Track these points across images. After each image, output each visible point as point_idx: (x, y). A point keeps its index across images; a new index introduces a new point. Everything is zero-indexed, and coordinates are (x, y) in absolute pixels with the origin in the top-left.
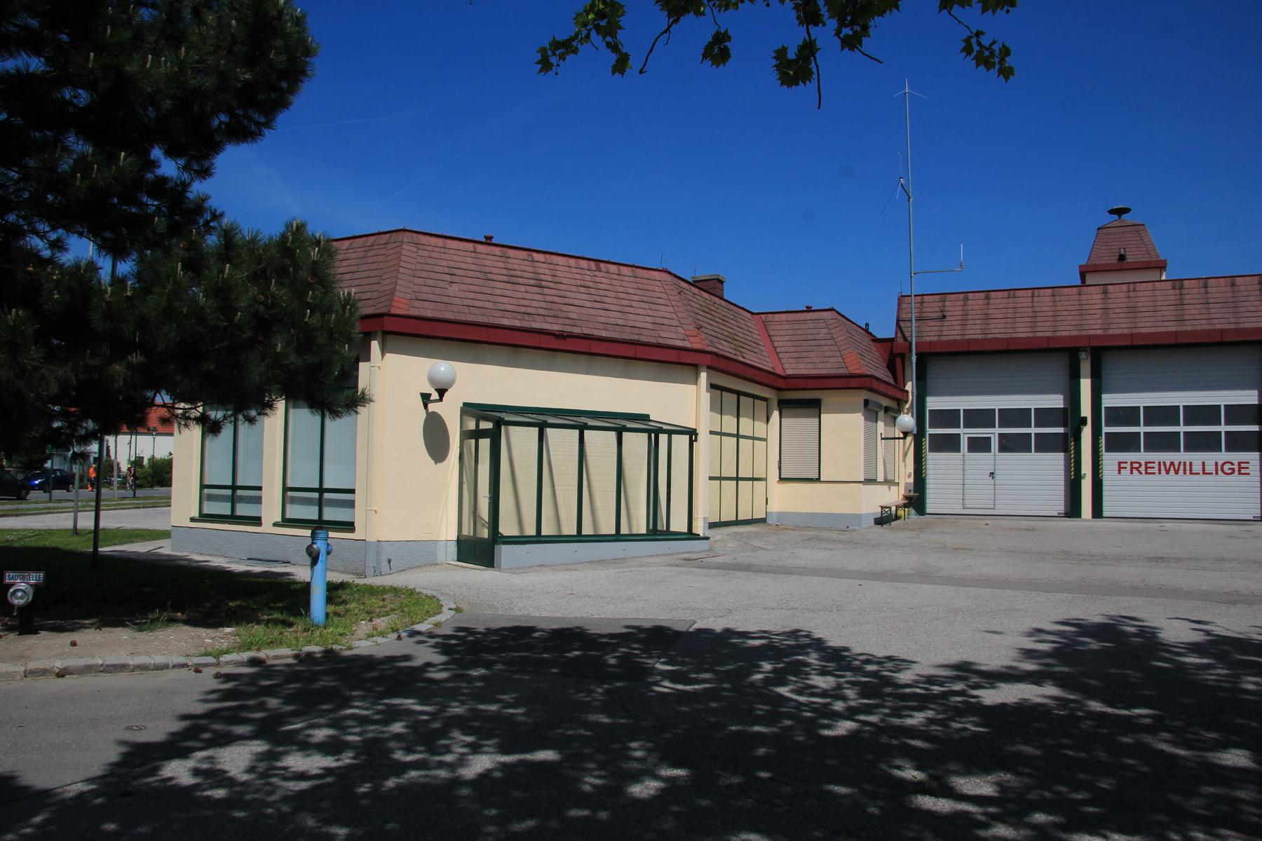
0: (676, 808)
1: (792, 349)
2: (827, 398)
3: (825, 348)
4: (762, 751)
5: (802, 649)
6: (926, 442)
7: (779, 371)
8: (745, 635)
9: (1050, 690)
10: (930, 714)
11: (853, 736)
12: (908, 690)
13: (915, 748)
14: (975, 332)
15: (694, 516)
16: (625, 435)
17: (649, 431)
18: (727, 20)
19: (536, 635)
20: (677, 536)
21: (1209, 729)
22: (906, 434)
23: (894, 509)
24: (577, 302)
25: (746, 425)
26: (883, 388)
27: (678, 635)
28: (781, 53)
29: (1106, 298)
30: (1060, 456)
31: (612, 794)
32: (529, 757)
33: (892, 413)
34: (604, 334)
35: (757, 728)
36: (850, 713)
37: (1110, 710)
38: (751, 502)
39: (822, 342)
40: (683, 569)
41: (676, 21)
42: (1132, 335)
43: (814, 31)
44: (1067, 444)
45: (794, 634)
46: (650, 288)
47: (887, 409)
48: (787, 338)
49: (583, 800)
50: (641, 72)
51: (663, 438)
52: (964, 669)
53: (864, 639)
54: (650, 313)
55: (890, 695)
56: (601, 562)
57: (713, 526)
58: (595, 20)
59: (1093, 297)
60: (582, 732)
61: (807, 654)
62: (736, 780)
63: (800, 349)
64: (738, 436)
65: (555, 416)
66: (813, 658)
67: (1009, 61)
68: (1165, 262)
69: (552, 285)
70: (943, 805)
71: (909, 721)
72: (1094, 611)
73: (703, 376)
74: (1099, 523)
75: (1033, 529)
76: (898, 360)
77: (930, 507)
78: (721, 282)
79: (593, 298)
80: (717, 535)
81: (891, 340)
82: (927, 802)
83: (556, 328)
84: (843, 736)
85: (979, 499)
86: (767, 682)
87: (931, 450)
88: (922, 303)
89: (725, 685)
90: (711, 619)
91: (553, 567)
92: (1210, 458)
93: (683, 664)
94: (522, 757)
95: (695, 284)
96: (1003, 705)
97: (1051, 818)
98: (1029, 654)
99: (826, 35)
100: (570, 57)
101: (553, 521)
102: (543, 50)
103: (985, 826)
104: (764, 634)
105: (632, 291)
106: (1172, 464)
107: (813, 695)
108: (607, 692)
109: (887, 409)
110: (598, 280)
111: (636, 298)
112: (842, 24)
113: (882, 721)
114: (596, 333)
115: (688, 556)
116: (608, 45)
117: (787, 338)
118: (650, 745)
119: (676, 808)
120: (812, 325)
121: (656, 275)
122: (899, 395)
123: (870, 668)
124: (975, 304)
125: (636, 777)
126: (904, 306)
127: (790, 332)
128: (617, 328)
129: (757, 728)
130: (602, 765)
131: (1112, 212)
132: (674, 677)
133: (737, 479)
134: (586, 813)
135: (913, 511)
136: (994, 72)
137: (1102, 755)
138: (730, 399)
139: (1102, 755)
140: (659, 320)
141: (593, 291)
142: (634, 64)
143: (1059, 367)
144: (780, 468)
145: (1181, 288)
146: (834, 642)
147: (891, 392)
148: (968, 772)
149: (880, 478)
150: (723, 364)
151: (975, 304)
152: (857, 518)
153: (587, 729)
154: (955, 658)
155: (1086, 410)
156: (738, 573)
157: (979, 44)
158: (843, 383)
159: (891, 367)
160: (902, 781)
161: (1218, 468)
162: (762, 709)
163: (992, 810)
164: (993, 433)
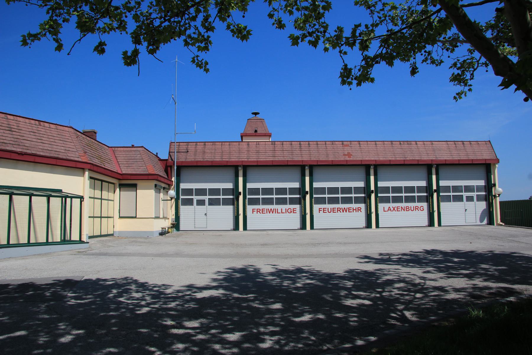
0: (80, 344)
1: (125, 163)
2: (140, 183)
3: (139, 163)
4: (113, 321)
5: (129, 284)
6: (180, 202)
7: (119, 172)
8: (105, 280)
9: (221, 291)
10: (177, 303)
11: (149, 312)
12: (170, 296)
13: (172, 314)
14: (199, 158)
15: (82, 233)
16: (51, 198)
17: (62, 197)
18: (105, 37)
19: (10, 287)
20: (75, 242)
21: (271, 299)
22: (172, 198)
23: (167, 229)
24: (29, 139)
25: (105, 194)
26: (162, 180)
27: (77, 282)
28: (125, 53)
29: (248, 147)
30: (231, 207)
31: (53, 342)
32: (12, 335)
33: (166, 190)
34: (42, 154)
35: (111, 313)
36: (148, 305)
37: (240, 296)
38: (107, 227)
39: (138, 160)
40: (78, 256)
41: (85, 35)
42: (257, 161)
43: (138, 47)
44: (234, 202)
45: (126, 278)
46: (63, 134)
47: (164, 188)
48: (123, 158)
49: (39, 347)
50: (68, 54)
51: (68, 200)
52: (190, 287)
53: (153, 279)
54: (63, 145)
55: (163, 297)
56: (40, 255)
57: (90, 237)
58: (49, 28)
59: (244, 146)
60: (37, 322)
61: (131, 286)
62: (103, 332)
63: (128, 163)
64: (101, 199)
65: (17, 190)
66: (133, 287)
67: (208, 67)
68: (271, 134)
69: (17, 130)
70: (181, 331)
71: (170, 306)
72: (239, 264)
73: (87, 173)
74: (246, 232)
75: (221, 235)
76: (169, 168)
77: (182, 227)
78: (96, 133)
79: (37, 137)
80: (92, 241)
81: (167, 160)
82: (175, 331)
83: (18, 150)
84: (145, 313)
85: (201, 224)
86: (115, 297)
87: (182, 205)
88: (179, 145)
89: (98, 299)
90: (91, 275)
91: (15, 258)
92: (284, 207)
93: (79, 293)
94: (9, 335)
95: (84, 133)
96: (204, 298)
97: (217, 331)
98: (215, 280)
99: (143, 48)
100: (36, 42)
101: (15, 237)
102: (24, 36)
103: (195, 336)
104: (113, 279)
105: (55, 135)
106: (271, 209)
107: (133, 300)
108: (47, 306)
109: (164, 188)
110: (39, 129)
111: (57, 138)
112: (149, 45)
113: (160, 306)
114: (38, 153)
115: (79, 250)
116: (54, 39)
117: (123, 158)
118: (67, 324)
119: (80, 344)
120: (134, 153)
121: (67, 129)
122: (169, 182)
123: (155, 289)
124: (200, 147)
125: (62, 335)
126: (172, 146)
127: (125, 156)
128: (48, 151)
129: (111, 313)
130: (47, 333)
131: (253, 113)
132: (76, 298)
133: (101, 217)
134: (42, 351)
135: (174, 229)
136: (202, 70)
137: (236, 310)
138: (98, 183)
139: (236, 310)
140: (67, 149)
141: (37, 134)
142: (66, 48)
143: (230, 173)
144: (119, 212)
145: (274, 144)
146: (142, 280)
147: (166, 181)
148: (190, 320)
149: (161, 216)
150: (95, 169)
151: (200, 147)
152: (152, 233)
153: (39, 321)
154: (188, 283)
155: (241, 189)
156: (102, 257)
157: (198, 60)
158: (146, 177)
159: (166, 171)
160: (166, 325)
161: (287, 211)
162: (113, 306)
163: (198, 331)
164: (206, 198)
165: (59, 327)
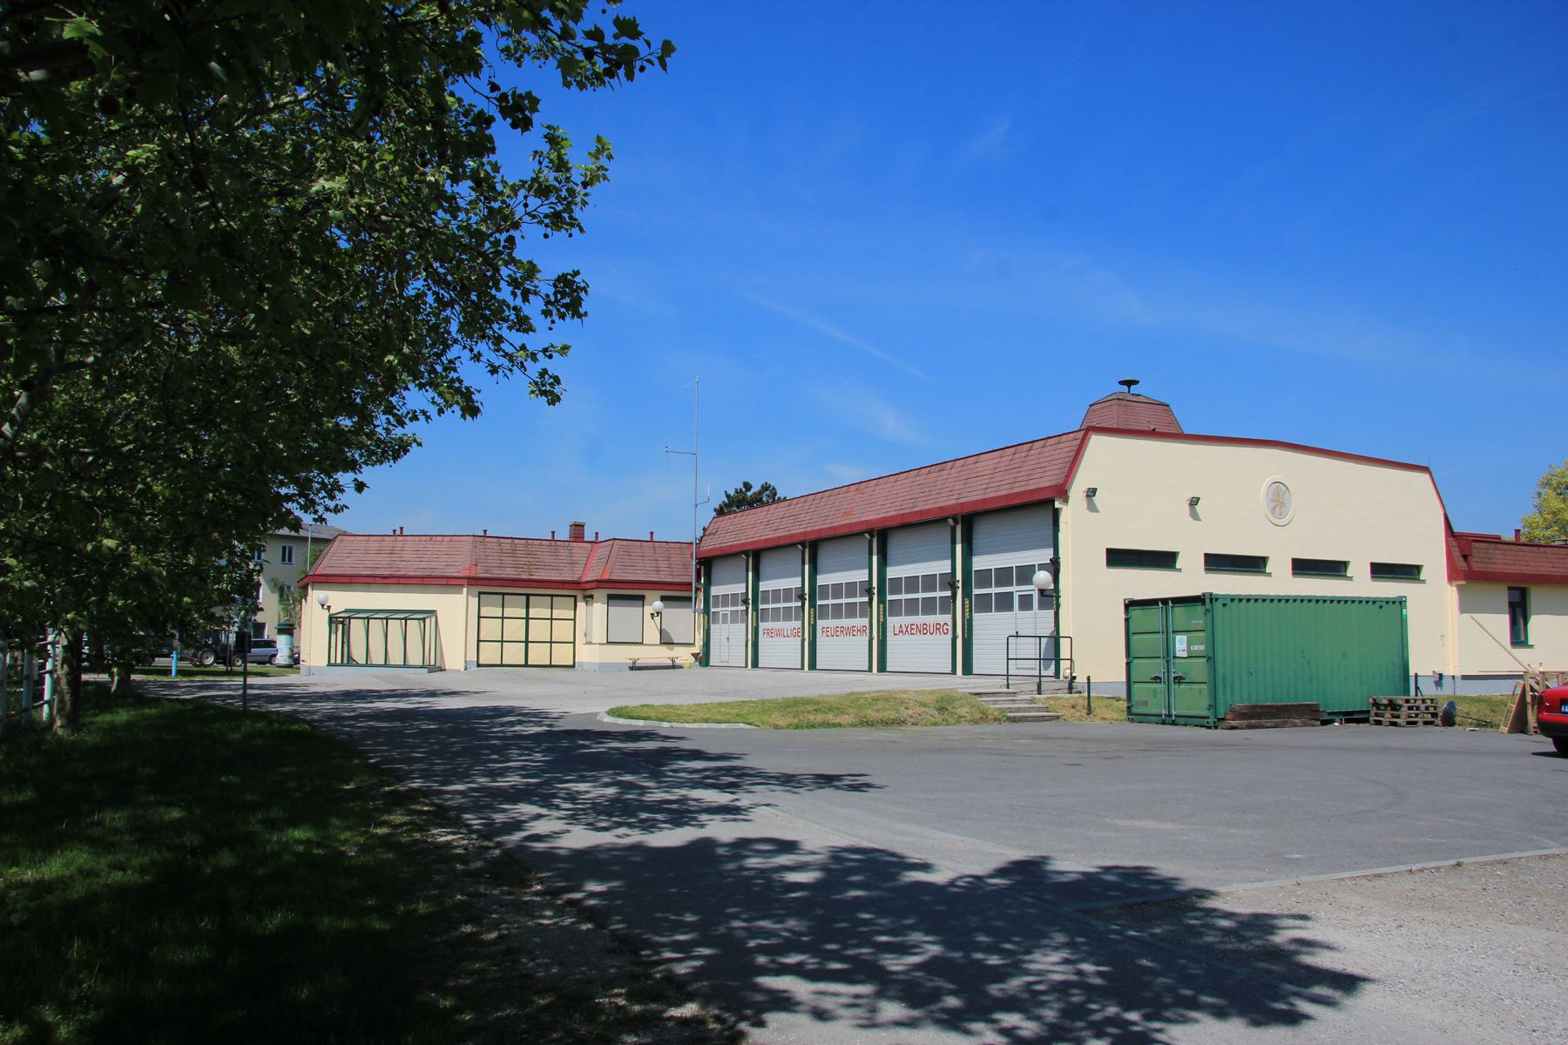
131: (1122, 383)
133: (527, 642)
165: (1026, 966)
